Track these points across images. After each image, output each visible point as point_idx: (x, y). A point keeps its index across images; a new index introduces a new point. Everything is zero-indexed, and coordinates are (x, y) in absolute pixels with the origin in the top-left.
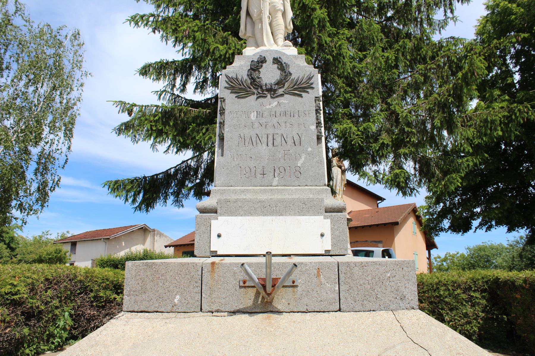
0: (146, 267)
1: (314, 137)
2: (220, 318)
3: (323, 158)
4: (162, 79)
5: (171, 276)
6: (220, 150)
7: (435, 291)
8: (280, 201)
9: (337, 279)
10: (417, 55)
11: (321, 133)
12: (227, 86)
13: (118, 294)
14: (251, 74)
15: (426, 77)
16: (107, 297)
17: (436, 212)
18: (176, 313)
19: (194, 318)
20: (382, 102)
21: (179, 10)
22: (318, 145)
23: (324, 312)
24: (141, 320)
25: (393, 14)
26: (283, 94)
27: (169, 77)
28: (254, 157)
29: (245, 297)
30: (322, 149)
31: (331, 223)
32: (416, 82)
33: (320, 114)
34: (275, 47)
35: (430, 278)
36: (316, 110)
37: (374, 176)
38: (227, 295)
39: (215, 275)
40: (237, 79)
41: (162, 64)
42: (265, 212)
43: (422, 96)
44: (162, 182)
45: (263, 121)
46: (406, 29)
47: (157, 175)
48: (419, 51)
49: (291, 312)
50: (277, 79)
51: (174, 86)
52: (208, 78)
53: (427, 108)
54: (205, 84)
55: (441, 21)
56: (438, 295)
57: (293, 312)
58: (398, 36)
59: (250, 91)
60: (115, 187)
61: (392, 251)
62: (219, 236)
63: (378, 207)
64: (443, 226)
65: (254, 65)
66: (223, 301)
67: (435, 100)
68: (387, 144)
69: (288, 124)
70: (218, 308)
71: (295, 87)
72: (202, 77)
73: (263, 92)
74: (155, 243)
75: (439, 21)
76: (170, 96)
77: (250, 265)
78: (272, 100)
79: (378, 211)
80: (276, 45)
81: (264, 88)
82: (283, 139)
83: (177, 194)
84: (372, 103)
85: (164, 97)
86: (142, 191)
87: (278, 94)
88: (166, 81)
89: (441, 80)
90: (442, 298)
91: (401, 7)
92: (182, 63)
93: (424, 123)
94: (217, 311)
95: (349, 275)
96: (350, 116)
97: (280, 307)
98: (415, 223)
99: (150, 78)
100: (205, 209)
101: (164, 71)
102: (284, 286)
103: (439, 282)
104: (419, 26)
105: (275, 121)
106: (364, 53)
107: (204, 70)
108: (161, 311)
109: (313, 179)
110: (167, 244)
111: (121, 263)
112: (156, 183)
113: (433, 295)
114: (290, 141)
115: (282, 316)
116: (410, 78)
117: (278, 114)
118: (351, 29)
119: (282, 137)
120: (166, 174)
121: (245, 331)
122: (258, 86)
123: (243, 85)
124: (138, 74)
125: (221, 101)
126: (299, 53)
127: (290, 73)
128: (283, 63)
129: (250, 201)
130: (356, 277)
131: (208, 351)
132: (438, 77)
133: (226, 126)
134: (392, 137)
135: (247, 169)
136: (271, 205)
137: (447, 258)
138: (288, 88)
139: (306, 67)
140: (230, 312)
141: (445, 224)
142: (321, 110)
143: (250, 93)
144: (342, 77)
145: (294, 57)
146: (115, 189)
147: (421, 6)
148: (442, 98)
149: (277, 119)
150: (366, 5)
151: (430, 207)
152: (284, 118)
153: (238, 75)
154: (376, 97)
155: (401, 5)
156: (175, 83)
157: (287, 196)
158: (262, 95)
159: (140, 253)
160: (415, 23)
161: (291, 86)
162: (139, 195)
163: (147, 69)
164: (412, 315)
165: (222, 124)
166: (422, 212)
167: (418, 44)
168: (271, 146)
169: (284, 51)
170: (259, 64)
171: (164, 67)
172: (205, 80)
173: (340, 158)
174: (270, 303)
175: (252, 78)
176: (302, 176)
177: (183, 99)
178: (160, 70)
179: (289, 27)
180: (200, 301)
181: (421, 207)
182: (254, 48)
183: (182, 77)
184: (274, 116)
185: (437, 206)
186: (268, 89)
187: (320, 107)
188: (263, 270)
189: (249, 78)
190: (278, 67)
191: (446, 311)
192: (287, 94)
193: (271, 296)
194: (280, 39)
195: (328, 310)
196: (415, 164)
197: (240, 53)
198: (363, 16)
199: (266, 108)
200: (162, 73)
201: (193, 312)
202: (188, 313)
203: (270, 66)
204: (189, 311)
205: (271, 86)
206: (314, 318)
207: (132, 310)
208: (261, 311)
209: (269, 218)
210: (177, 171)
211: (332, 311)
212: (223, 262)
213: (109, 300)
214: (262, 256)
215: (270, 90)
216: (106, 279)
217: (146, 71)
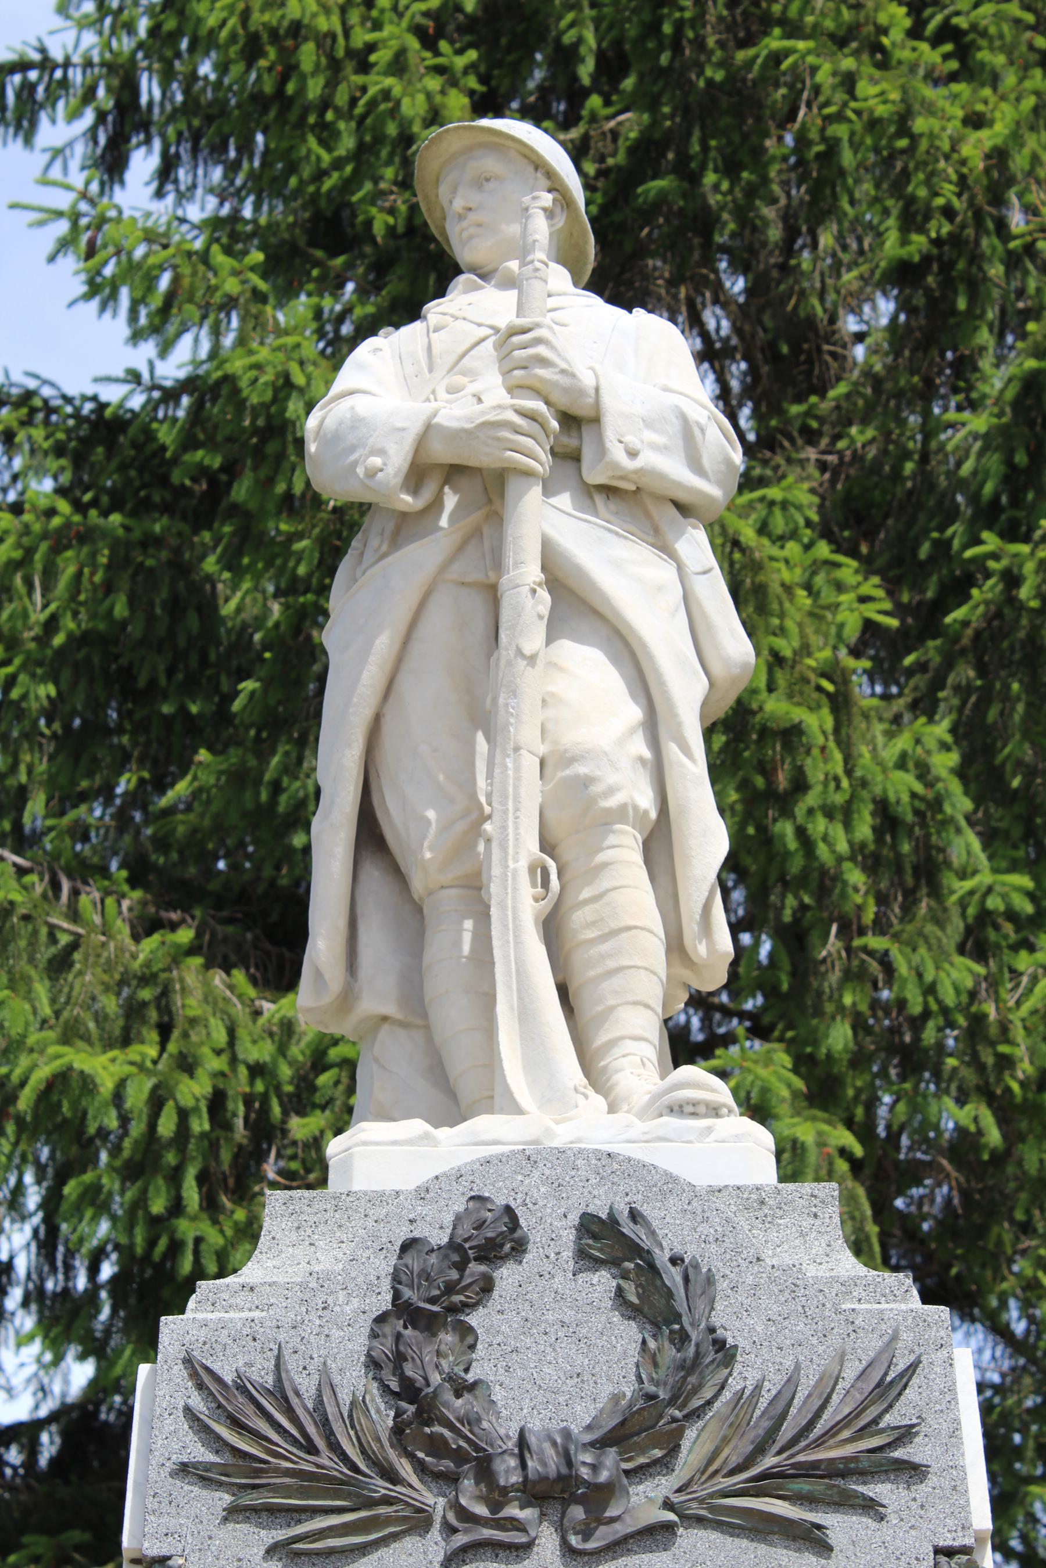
12: (201, 1453)
14: (400, 1358)
26: (668, 1528)
40: (281, 1395)
50: (616, 1398)
59: (387, 1501)
71: (769, 1461)
73: (496, 1507)
80: (598, 1101)
81: (508, 1474)
87: (620, 1529)
122: (459, 1457)
123: (335, 1447)
127: (720, 1345)
128: (661, 1258)
138: (707, 1470)
139: (847, 1286)
153: (292, 1363)
158: (487, 1533)
161: (733, 1455)
170: (461, 1266)
175: (409, 1391)
179: (702, 949)
182: (418, 1126)
189: (385, 1389)
192: (700, 1521)
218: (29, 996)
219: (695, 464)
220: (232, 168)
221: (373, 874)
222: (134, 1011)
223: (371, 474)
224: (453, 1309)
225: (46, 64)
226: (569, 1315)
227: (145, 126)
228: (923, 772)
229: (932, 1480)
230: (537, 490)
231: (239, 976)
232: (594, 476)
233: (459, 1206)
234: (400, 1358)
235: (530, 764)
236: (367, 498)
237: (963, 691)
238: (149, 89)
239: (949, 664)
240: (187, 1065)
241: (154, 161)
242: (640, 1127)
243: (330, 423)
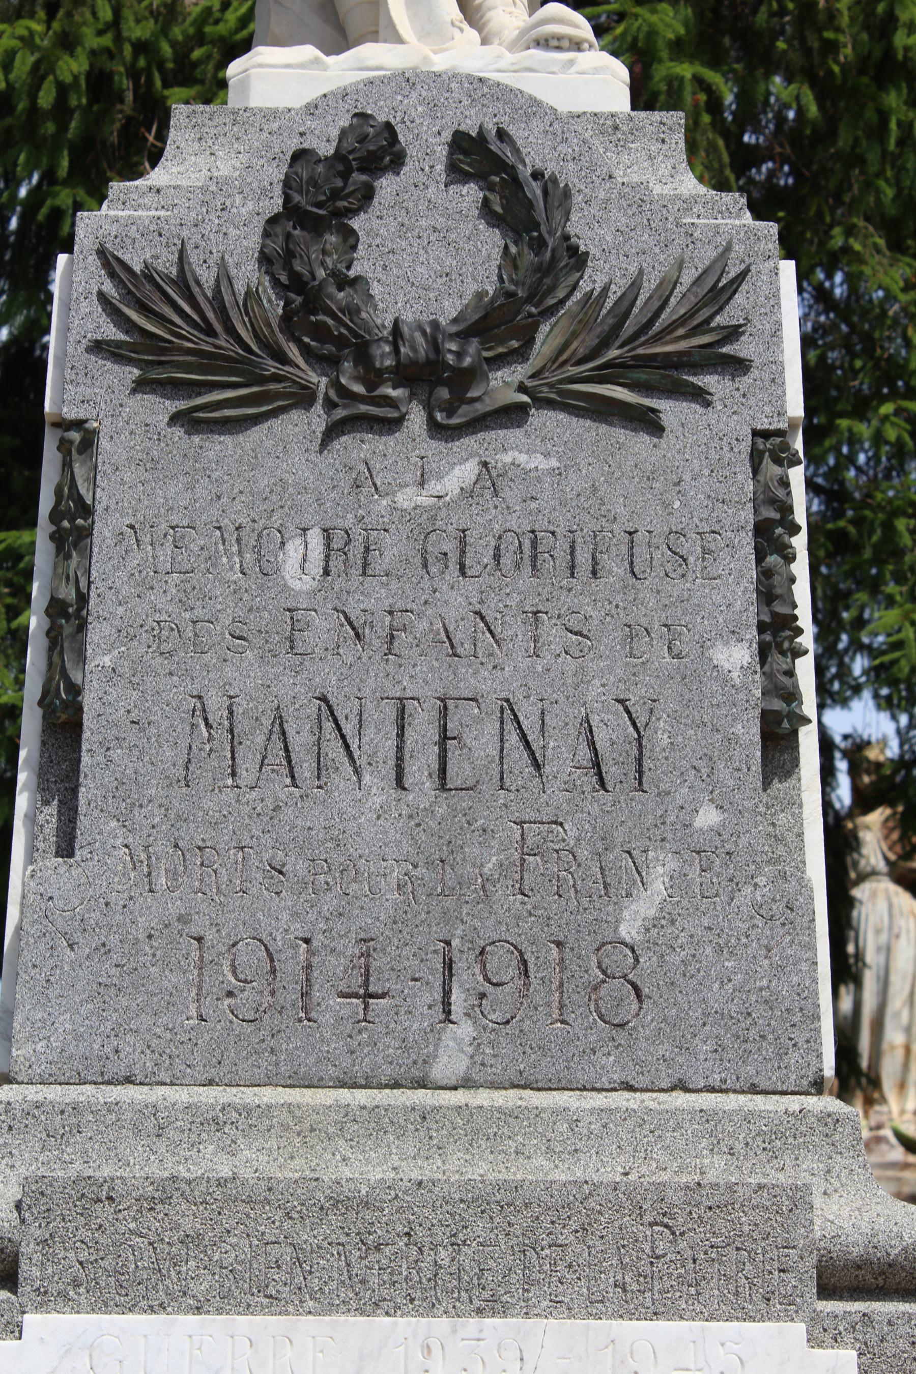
1: (739, 729)
3: (804, 886)
6: (52, 809)
11: (792, 696)
12: (112, 332)
14: (289, 255)
22: (766, 784)
28: (298, 866)
30: (799, 819)
33: (790, 558)
36: (762, 530)
42: (374, 1281)
45: (370, 604)
50: (480, 295)
59: (277, 378)
65: (313, 181)
71: (613, 353)
73: (371, 386)
80: (473, 35)
82: (513, 738)
87: (480, 408)
109: (728, 1040)
119: (510, 726)
122: (341, 342)
123: (231, 330)
125: (64, 446)
127: (573, 250)
128: (252, 26)
133: (97, 633)
136: (420, 1232)
138: (557, 359)
139: (689, 203)
142: (794, 529)
143: (278, 396)
149: (470, 587)
153: (194, 257)
157: (540, 1161)
158: (363, 408)
161: (579, 347)
170: (345, 176)
176: (650, 1013)
182: (309, 51)
184: (454, 567)
186: (414, 363)
187: (786, 509)
190: (486, 202)
192: (550, 404)
203: (431, 192)
205: (435, 345)
226: (441, 222)
229: (754, 373)
234: (289, 255)
242: (509, 58)
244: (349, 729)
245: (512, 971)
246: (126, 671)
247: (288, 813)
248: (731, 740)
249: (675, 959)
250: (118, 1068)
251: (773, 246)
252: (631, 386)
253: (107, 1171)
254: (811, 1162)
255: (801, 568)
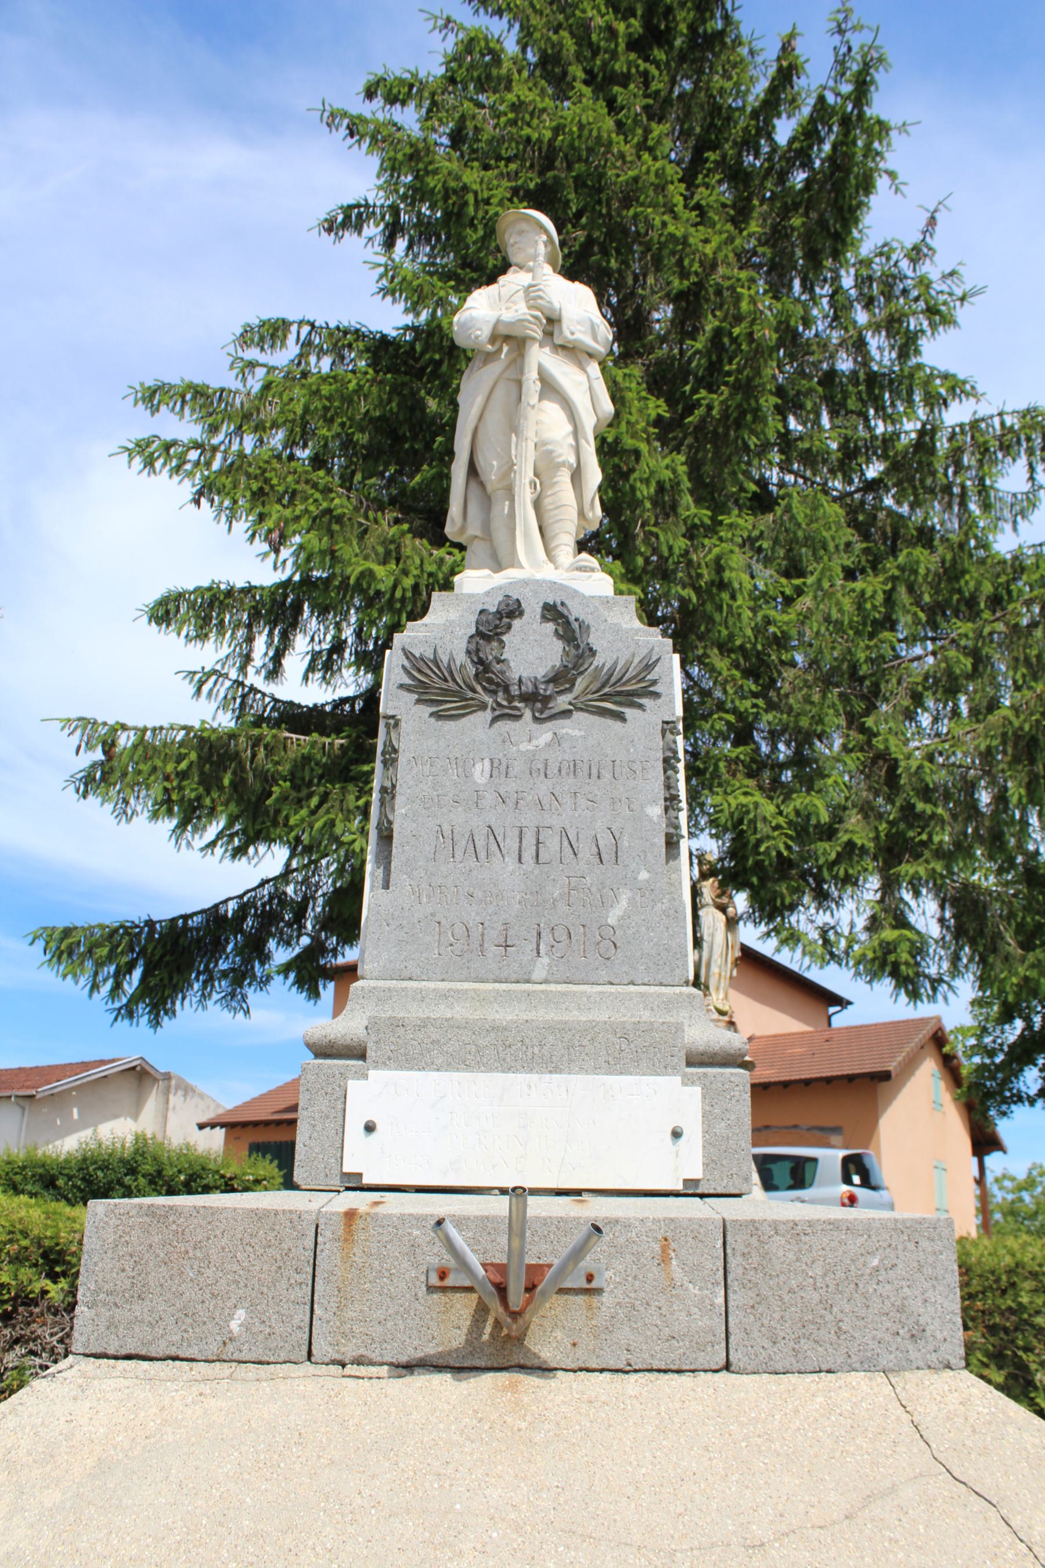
0: (148, 1219)
2: (366, 1382)
3: (682, 903)
4: (212, 639)
5: (223, 1248)
7: (1004, 1292)
8: (551, 1028)
9: (721, 1272)
10: (954, 591)
11: (677, 827)
12: (407, 681)
13: (54, 1277)
14: (478, 650)
15: (979, 660)
16: (21, 1288)
17: (1001, 1045)
18: (234, 1364)
19: (289, 1381)
20: (849, 728)
21: (273, 442)
22: (667, 862)
23: (679, 1371)
24: (126, 1383)
25: (882, 473)
26: (570, 712)
27: (233, 633)
28: (479, 894)
29: (443, 1321)
31: (704, 1097)
32: (949, 673)
33: (677, 772)
34: (547, 572)
35: (990, 1254)
36: (666, 760)
37: (820, 942)
38: (390, 1311)
39: (355, 1250)
40: (436, 661)
41: (214, 595)
43: (964, 709)
44: (199, 940)
46: (919, 515)
47: (186, 917)
48: (957, 579)
49: (581, 1370)
50: (554, 667)
51: (247, 659)
52: (345, 641)
53: (983, 747)
54: (335, 657)
55: (1019, 496)
56: (1013, 1305)
57: (588, 1370)
58: (896, 536)
59: (472, 699)
60: (63, 947)
61: (871, 1161)
62: (370, 1128)
63: (830, 1024)
64: (1023, 1089)
65: (488, 622)
66: (377, 1331)
67: (1004, 726)
68: (863, 846)
69: (582, 801)
70: (362, 1351)
71: (606, 690)
72: (329, 638)
73: (510, 702)
74: (170, 1114)
75: (1014, 495)
76: (229, 689)
77: (461, 1222)
78: (535, 726)
79: (829, 1035)
80: (551, 566)
81: (515, 690)
82: (566, 843)
83: (240, 977)
84: (819, 729)
85: (211, 690)
86: (141, 962)
87: (553, 711)
88: (225, 645)
89: (1024, 670)
90: (1025, 1316)
91: (907, 453)
92: (273, 593)
93: (970, 787)
94: (359, 1361)
95: (755, 1259)
96: (755, 767)
97: (547, 1354)
98: (938, 1074)
99: (179, 634)
100: (331, 1045)
101: (218, 615)
102: (563, 1291)
103: (1017, 1265)
104: (956, 509)
105: (543, 787)
106: (797, 582)
107: (335, 616)
108: (187, 1355)
109: (651, 965)
110: (203, 1119)
111: (66, 1172)
112: (181, 941)
113: (999, 1307)
114: (587, 851)
115: (553, 1383)
116: (930, 660)
117: (553, 770)
118: (763, 513)
119: (565, 839)
120: (214, 915)
121: (441, 1426)
122: (498, 685)
123: (454, 680)
124: (145, 619)
125: (387, 725)
126: (619, 592)
127: (591, 649)
128: (572, 619)
129: (466, 1025)
130: (778, 1267)
131: (327, 1489)
132: (1016, 659)
133: (399, 800)
134: (876, 828)
135: (459, 930)
136: (527, 1041)
137: (1034, 1181)
138: (584, 692)
139: (637, 631)
140: (397, 1366)
141: (1029, 1082)
142: (679, 760)
144: (731, 651)
145: (605, 601)
146: (62, 952)
147: (963, 452)
148: (1025, 721)
150: (807, 445)
151: (984, 1030)
152: (569, 783)
153: (440, 651)
154: (831, 711)
155: (906, 447)
156: (251, 650)
157: (576, 1013)
158: (507, 711)
159: (123, 1146)
160: (946, 499)
161: (594, 687)
162: (130, 973)
163: (171, 607)
164: (946, 1388)
165: (388, 793)
166: (960, 1046)
167: (954, 560)
168: (532, 862)
169: (575, 585)
170: (500, 619)
171: (221, 602)
172: (338, 647)
173: (723, 885)
174: (520, 1339)
175: (481, 662)
177: (267, 700)
178: (208, 611)
179: (591, 515)
180: (307, 1330)
181: (961, 1030)
182: (486, 572)
183: (271, 634)
185: (1007, 1027)
187: (675, 752)
188: (499, 1240)
189: (472, 661)
191: (1038, 1355)
192: (581, 709)
193: (520, 1321)
194: (563, 547)
195: (692, 1367)
196: (942, 907)
197: (447, 586)
198: (797, 474)
199: (518, 751)
200: (214, 622)
201: (285, 1362)
202: (268, 1363)
204: (272, 1359)
205: (536, 687)
206: (649, 1392)
207: (99, 1350)
208: (489, 1364)
209: (520, 1079)
210: (243, 909)
211: (705, 1371)
212: (380, 1209)
213: (27, 1297)
214: (497, 1192)
215: (531, 698)
216: (21, 1232)
217: (167, 612)
218: (351, 545)
219: (595, 338)
220: (433, 248)
221: (474, 486)
222: (388, 553)
223: (477, 337)
224: (497, 634)
225: (367, 206)
226: (538, 637)
227: (402, 230)
228: (674, 471)
229: (663, 698)
230: (537, 345)
231: (425, 541)
232: (558, 341)
233: (500, 598)
234: (478, 650)
235: (531, 445)
236: (475, 347)
237: (690, 447)
238: (404, 217)
239: (685, 438)
240: (405, 573)
241: (406, 243)
242: (566, 575)
243: (462, 319)
244: (499, 839)
245: (565, 937)
246: (411, 814)
247: (475, 872)
248: (653, 845)
249: (630, 932)
250: (406, 974)
251: (671, 648)
252: (615, 703)
253: (401, 1015)
254: (684, 1013)
255: (681, 776)
